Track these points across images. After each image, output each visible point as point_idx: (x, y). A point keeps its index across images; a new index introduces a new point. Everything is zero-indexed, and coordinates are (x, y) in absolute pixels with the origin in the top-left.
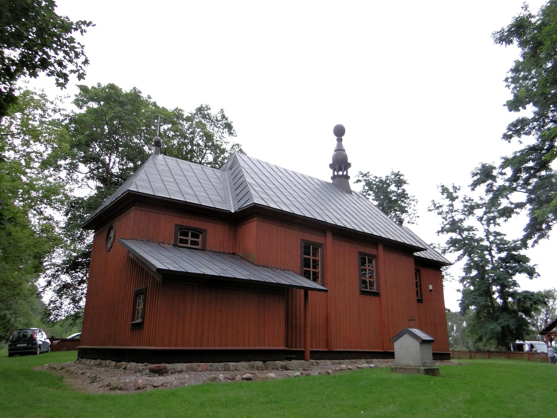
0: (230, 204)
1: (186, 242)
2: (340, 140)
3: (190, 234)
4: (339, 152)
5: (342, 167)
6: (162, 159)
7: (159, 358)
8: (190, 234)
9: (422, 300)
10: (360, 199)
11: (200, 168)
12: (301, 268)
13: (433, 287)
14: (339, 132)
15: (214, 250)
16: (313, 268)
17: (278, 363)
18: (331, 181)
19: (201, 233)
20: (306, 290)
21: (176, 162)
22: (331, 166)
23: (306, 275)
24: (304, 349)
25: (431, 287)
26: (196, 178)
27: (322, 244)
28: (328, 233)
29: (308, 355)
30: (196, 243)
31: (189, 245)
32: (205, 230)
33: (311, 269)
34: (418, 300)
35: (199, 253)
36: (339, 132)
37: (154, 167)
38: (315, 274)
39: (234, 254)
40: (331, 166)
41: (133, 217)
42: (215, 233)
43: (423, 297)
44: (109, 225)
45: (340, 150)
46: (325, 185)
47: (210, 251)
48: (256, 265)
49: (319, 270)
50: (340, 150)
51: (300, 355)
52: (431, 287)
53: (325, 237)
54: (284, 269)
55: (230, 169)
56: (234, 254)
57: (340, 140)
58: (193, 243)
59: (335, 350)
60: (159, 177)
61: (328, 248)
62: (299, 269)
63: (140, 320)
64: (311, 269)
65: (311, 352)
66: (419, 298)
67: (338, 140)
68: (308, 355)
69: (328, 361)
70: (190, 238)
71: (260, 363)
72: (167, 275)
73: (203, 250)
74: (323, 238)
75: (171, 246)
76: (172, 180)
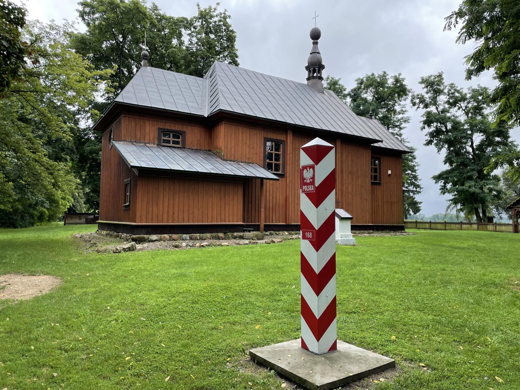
0: (205, 109)
1: (169, 142)
2: (315, 43)
3: (171, 135)
4: (313, 54)
5: (317, 69)
6: (150, 71)
7: (141, 232)
8: (171, 135)
9: (380, 183)
10: (331, 98)
11: (184, 77)
12: (264, 161)
13: (392, 172)
14: (315, 36)
15: (195, 148)
16: (275, 160)
17: (235, 234)
18: (306, 82)
19: (181, 135)
20: (262, 179)
21: (162, 74)
22: (307, 68)
23: (269, 167)
24: (258, 223)
25: (390, 172)
26: (178, 88)
27: (284, 141)
28: (289, 133)
29: (262, 227)
30: (178, 143)
31: (171, 144)
32: (185, 132)
33: (274, 162)
34: (372, 182)
35: (178, 152)
36: (315, 36)
37: (142, 79)
38: (277, 166)
39: (210, 150)
40: (307, 68)
41: (126, 124)
42: (193, 135)
43: (382, 180)
44: (109, 130)
45: (315, 52)
46: (302, 85)
47: (189, 148)
48: (224, 160)
49: (280, 162)
50: (315, 52)
51: (257, 228)
52: (390, 172)
53: (287, 135)
54: (249, 163)
55: (210, 77)
56: (210, 151)
57: (315, 43)
58: (174, 142)
59: (293, 224)
60: (144, 88)
61: (288, 144)
62: (262, 162)
63: (127, 204)
64: (274, 162)
65: (265, 225)
66: (373, 181)
67: (314, 43)
68: (262, 227)
69: (285, 232)
70: (171, 139)
71: (221, 235)
72: (141, 169)
73: (183, 148)
74: (285, 136)
75: (156, 145)
76: (156, 90)
